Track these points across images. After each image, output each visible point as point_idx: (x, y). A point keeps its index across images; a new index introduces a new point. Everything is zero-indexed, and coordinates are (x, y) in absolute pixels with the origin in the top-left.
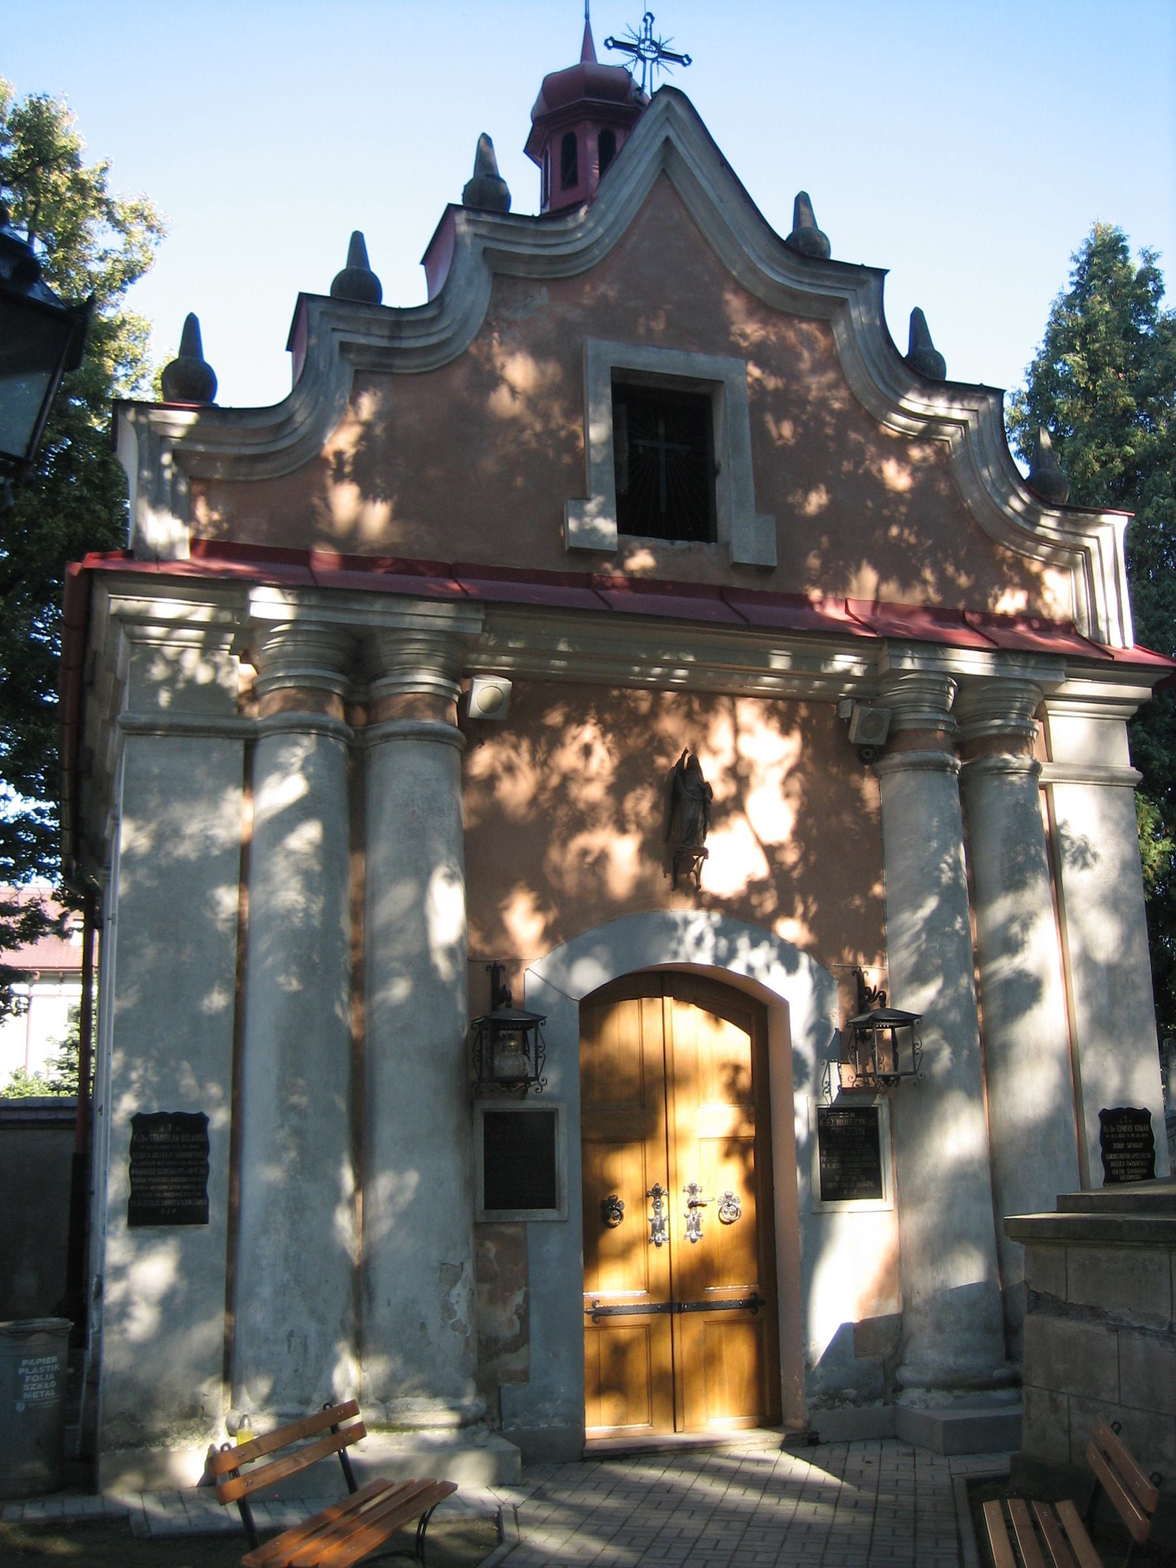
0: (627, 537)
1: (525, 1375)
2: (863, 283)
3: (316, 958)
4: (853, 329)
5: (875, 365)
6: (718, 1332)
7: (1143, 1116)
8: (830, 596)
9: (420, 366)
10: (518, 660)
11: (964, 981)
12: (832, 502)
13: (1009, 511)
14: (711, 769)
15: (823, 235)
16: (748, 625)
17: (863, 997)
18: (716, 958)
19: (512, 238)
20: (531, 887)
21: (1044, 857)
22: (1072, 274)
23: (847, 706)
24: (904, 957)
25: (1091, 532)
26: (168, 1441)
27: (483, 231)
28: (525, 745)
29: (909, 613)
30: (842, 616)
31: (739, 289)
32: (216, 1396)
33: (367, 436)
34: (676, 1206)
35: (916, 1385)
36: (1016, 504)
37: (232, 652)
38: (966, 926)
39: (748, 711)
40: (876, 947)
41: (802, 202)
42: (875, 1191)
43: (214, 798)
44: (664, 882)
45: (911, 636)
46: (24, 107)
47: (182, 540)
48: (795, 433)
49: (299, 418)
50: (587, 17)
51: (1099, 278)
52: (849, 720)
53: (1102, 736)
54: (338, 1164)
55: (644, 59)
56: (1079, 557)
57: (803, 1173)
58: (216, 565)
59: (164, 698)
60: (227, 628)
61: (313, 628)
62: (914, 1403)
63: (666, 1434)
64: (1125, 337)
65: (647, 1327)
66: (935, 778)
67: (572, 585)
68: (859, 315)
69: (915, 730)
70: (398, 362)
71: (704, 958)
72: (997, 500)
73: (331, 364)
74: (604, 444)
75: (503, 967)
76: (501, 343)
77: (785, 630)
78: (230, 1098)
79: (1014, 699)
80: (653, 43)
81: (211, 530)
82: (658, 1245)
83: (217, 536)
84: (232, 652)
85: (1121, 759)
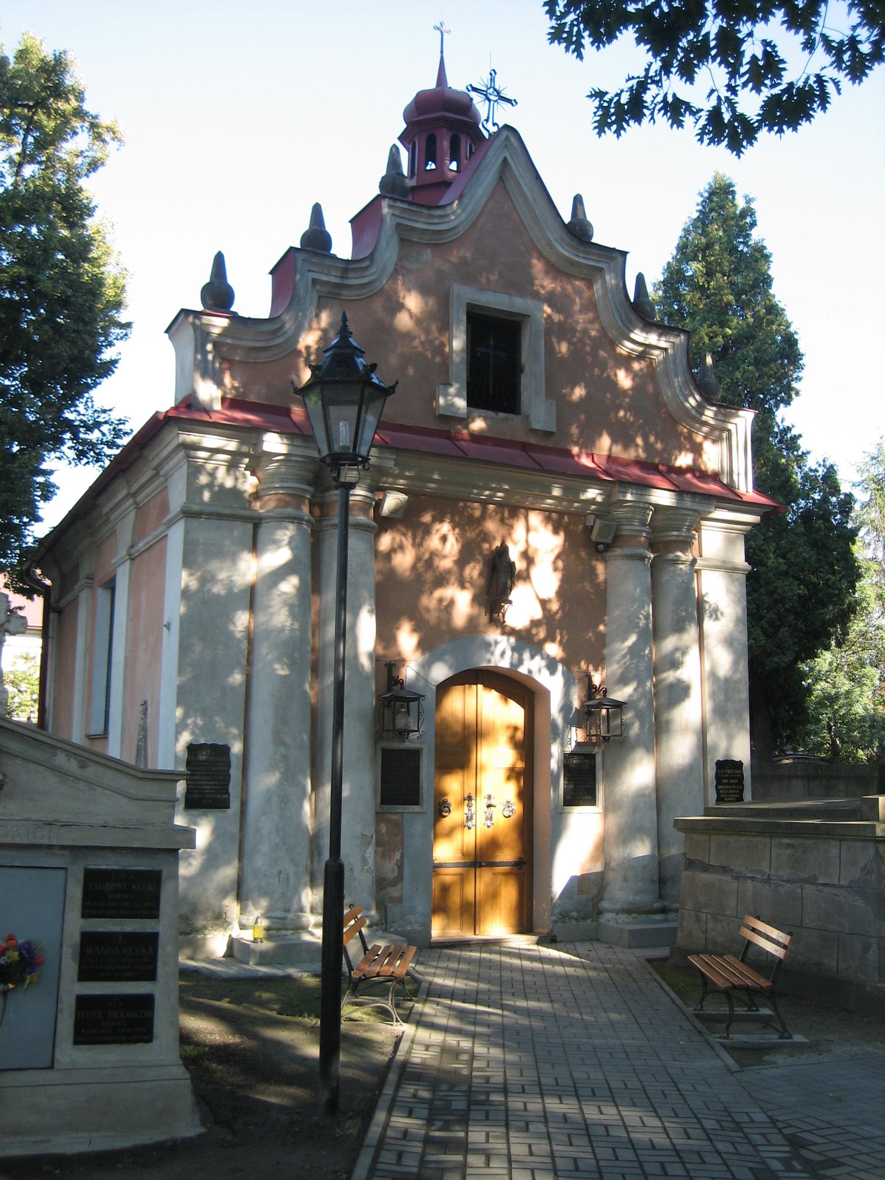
1: (400, 900)
2: (613, 259)
3: (296, 655)
4: (606, 287)
5: (618, 311)
6: (500, 878)
7: (739, 765)
8: (583, 451)
9: (358, 295)
11: (649, 684)
12: (588, 394)
13: (687, 405)
14: (514, 554)
16: (542, 469)
17: (590, 690)
18: (512, 664)
20: (411, 619)
21: (696, 614)
22: (698, 205)
24: (614, 668)
25: (732, 421)
26: (206, 932)
27: (397, 213)
28: (410, 534)
29: (627, 464)
30: (590, 464)
31: (541, 257)
32: (232, 907)
34: (480, 804)
36: (692, 402)
37: (246, 469)
38: (651, 652)
39: (535, 518)
40: (599, 661)
41: (578, 201)
42: (592, 802)
43: (234, 558)
44: (484, 619)
45: (631, 481)
46: (50, 58)
47: (216, 398)
48: (569, 350)
49: (287, 326)
50: (442, 52)
51: (716, 211)
52: (592, 527)
53: (730, 542)
54: (305, 778)
55: (489, 100)
56: (725, 435)
57: (554, 791)
58: (239, 415)
59: (206, 496)
60: (245, 455)
62: (609, 921)
63: (469, 935)
64: (731, 254)
65: (461, 875)
66: (637, 565)
68: (610, 279)
69: (630, 536)
70: (344, 292)
71: (505, 664)
72: (682, 398)
73: (306, 293)
74: (462, 351)
75: (394, 665)
76: (403, 284)
77: (563, 474)
78: (242, 736)
79: (686, 520)
80: (495, 90)
81: (233, 392)
82: (469, 828)
84: (246, 469)
85: (739, 558)
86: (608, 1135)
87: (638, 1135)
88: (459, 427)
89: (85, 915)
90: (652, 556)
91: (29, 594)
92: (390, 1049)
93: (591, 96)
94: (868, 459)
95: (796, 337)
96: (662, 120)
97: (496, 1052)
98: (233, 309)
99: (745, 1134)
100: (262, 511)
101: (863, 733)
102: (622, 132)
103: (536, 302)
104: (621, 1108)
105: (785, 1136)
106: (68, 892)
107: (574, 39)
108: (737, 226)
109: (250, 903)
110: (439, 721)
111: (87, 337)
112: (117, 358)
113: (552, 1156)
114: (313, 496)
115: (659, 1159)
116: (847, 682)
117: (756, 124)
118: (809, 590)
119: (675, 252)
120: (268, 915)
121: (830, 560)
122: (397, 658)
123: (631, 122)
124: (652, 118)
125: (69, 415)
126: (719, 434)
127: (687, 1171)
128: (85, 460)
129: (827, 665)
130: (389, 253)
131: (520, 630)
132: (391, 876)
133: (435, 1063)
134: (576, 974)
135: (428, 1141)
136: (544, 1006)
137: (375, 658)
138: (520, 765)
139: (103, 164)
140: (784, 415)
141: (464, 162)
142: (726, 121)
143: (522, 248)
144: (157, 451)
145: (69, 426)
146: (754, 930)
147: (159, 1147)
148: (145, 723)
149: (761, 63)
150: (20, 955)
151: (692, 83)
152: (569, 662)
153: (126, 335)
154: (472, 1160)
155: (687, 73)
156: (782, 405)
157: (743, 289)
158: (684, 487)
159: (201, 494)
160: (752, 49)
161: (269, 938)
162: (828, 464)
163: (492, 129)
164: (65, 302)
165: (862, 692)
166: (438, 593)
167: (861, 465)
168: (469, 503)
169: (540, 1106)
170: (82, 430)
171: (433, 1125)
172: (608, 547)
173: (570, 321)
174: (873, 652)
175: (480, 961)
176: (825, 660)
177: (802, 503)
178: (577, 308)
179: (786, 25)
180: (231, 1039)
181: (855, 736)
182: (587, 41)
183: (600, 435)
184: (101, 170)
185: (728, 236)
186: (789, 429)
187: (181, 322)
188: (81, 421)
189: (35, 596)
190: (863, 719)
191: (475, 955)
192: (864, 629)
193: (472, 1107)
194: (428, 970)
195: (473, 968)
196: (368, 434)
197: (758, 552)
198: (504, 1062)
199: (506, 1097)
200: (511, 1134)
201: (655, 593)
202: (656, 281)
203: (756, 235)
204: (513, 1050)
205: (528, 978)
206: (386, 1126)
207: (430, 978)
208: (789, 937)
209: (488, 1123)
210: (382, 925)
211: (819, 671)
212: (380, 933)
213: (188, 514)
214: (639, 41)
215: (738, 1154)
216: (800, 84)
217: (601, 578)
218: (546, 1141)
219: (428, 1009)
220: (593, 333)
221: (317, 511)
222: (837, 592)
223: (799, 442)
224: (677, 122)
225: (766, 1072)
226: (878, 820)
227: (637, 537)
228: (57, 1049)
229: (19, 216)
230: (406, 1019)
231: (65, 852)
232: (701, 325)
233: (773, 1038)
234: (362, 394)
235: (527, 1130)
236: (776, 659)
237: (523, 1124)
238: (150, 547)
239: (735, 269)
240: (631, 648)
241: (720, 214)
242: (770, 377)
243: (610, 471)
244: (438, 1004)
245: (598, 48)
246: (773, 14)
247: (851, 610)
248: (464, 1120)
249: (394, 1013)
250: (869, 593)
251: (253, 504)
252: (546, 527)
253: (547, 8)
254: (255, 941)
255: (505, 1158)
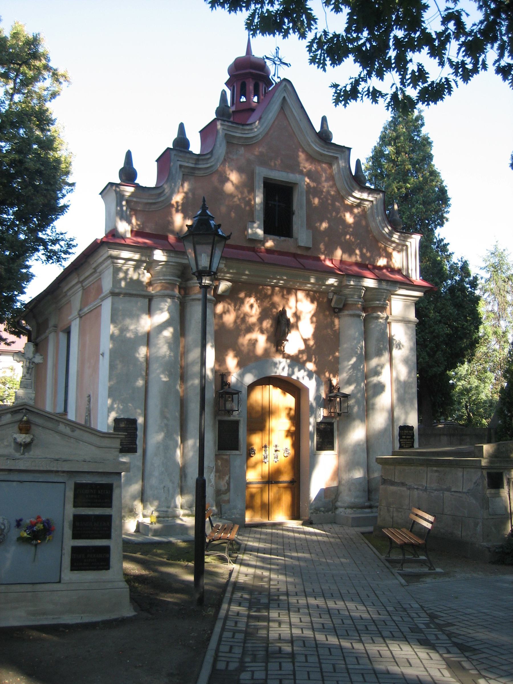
0: (266, 235)
1: (228, 501)
3: (172, 370)
5: (346, 180)
6: (282, 490)
7: (412, 428)
8: (327, 257)
10: (232, 276)
12: (330, 226)
13: (384, 232)
14: (289, 314)
15: (331, 133)
16: (304, 268)
17: (331, 387)
18: (288, 374)
19: (235, 131)
20: (234, 350)
23: (331, 296)
24: (344, 375)
26: (125, 519)
27: (225, 128)
28: (233, 304)
29: (351, 264)
30: (331, 265)
31: (304, 151)
32: (139, 506)
33: (186, 198)
34: (271, 450)
35: (341, 507)
36: (386, 230)
39: (301, 295)
40: (336, 372)
41: (324, 120)
42: (332, 448)
43: (137, 317)
44: (273, 349)
47: (128, 231)
48: (319, 202)
49: (166, 191)
52: (332, 299)
53: (407, 307)
55: (275, 64)
58: (140, 240)
59: (123, 284)
61: (173, 264)
63: (266, 521)
66: (356, 319)
67: (248, 251)
68: (342, 163)
69: (352, 304)
70: (197, 172)
71: (285, 374)
74: (260, 204)
75: (225, 375)
76: (229, 167)
77: (316, 271)
79: (383, 295)
80: (279, 58)
81: (137, 227)
82: (265, 463)
83: (139, 229)
84: (144, 269)
85: (412, 315)
86: (339, 614)
87: (354, 614)
88: (259, 245)
89: (75, 506)
90: (364, 315)
91: (18, 334)
92: (227, 576)
93: (331, 87)
94: (489, 254)
95: (446, 188)
96: (368, 101)
97: (282, 577)
98: (136, 182)
99: (408, 613)
100: (153, 292)
101: (485, 409)
102: (347, 105)
103: (301, 176)
104: (346, 602)
105: (427, 614)
106: (67, 495)
107: (322, 61)
108: (414, 125)
109: (148, 503)
110: (249, 405)
111: (52, 192)
112: (68, 204)
113: (311, 622)
114: (181, 284)
115: (364, 624)
116: (476, 381)
117: (416, 101)
118: (452, 330)
119: (378, 141)
120: (158, 509)
121: (465, 314)
122: (226, 371)
123: (352, 100)
124: (362, 99)
125: (40, 235)
126: (402, 247)
127: (378, 628)
128: (51, 261)
129: (465, 371)
130: (221, 150)
131: (293, 356)
132: (223, 488)
133: (251, 582)
134: (323, 540)
135: (249, 617)
136: (307, 555)
137: (215, 371)
138: (293, 429)
139: (59, 94)
140: (440, 232)
141: (262, 97)
142: (400, 100)
143: (294, 146)
144: (96, 259)
145: (44, 243)
146: (417, 515)
147: (116, 620)
148: (89, 406)
149: (417, 74)
150: (44, 526)
151: (382, 80)
152: (319, 373)
153: (72, 190)
154: (271, 624)
155: (380, 75)
156: (438, 227)
157: (416, 162)
158: (383, 278)
159: (120, 283)
160: (412, 67)
161: (158, 522)
162: (464, 260)
163: (278, 80)
164: (39, 173)
165: (485, 386)
166: (249, 336)
167: (485, 257)
168: (265, 287)
169: (305, 602)
170: (50, 244)
171: (252, 610)
172: (341, 310)
173: (320, 186)
174: (492, 364)
175: (272, 534)
176: (464, 369)
177: (449, 282)
178: (323, 179)
179: (429, 55)
180: (144, 572)
181: (481, 412)
182: (328, 62)
183: (336, 249)
184: (58, 97)
185: (409, 132)
186: (442, 240)
187: (109, 189)
188: (49, 239)
189: (22, 336)
190: (485, 402)
191: (269, 531)
192: (486, 351)
193: (271, 602)
194: (244, 538)
195: (269, 537)
196: (216, 261)
197: (424, 309)
198: (286, 582)
199: (288, 597)
200: (291, 613)
201: (366, 335)
202: (368, 157)
203: (424, 131)
204: (290, 576)
205: (297, 542)
206: (228, 610)
207: (246, 542)
208: (434, 518)
209: (279, 609)
210: (220, 514)
211: (461, 375)
212: (218, 519)
213: (113, 294)
214: (355, 61)
215: (404, 621)
216: (438, 81)
217: (337, 327)
218: (309, 616)
219: (246, 557)
220: (332, 193)
221: (183, 292)
222: (468, 332)
223: (448, 247)
224: (375, 101)
225: (420, 585)
226: (483, 457)
227: (356, 304)
228: (62, 573)
229: (13, 125)
230: (235, 562)
231: (65, 474)
232: (393, 182)
233: (426, 570)
234: (214, 240)
235: (299, 611)
236: (434, 369)
237: (297, 609)
238: (92, 311)
239: (412, 150)
240: (353, 365)
241: (404, 119)
242: (431, 211)
243: (342, 269)
244: (251, 555)
245: (334, 67)
246: (423, 48)
247: (474, 343)
248: (267, 607)
249: (229, 559)
250: (489, 330)
251: (148, 288)
252: (307, 299)
253: (308, 49)
254: (152, 523)
255: (289, 624)
